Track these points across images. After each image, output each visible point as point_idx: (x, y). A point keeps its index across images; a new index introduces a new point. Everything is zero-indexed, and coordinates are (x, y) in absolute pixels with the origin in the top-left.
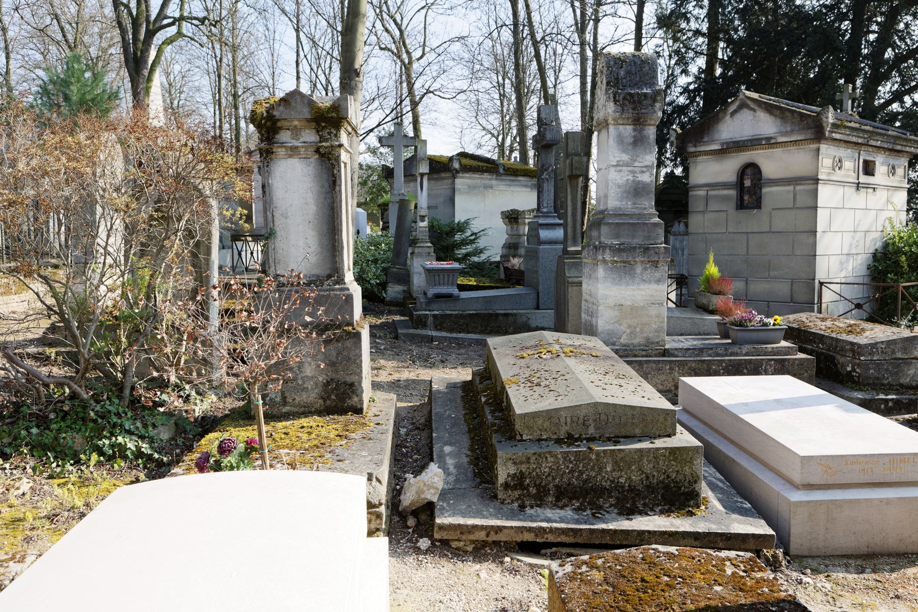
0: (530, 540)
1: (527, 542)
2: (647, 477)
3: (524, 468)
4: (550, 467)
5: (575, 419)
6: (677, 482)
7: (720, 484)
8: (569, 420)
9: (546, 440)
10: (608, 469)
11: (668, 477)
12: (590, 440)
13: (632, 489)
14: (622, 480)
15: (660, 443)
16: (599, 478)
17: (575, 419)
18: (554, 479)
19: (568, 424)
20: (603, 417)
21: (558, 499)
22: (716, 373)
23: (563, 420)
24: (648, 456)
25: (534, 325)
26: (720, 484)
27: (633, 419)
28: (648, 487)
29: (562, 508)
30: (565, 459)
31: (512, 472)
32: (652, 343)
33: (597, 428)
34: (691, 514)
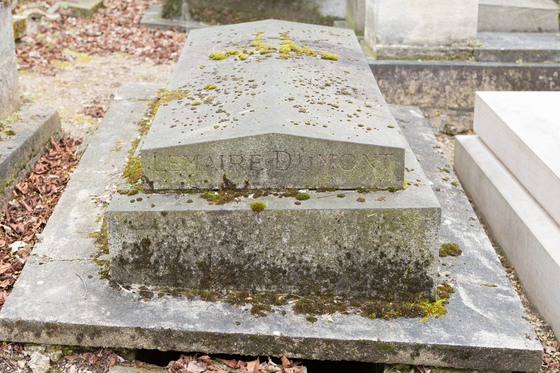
0: (146, 347)
1: (143, 350)
2: (348, 256)
3: (148, 234)
4: (190, 236)
5: (237, 159)
6: (396, 264)
7: (485, 262)
8: (227, 161)
9: (190, 191)
10: (285, 240)
11: (382, 255)
12: (258, 193)
13: (323, 273)
14: (307, 258)
15: (371, 202)
16: (270, 253)
17: (237, 159)
18: (197, 253)
19: (226, 167)
20: (283, 157)
21: (205, 284)
22: (544, 87)
23: (217, 161)
24: (349, 223)
25: (325, 12)
26: (485, 262)
27: (332, 161)
28: (350, 270)
29: (209, 298)
30: (214, 222)
31: (130, 241)
32: (456, 41)
33: (272, 175)
34: (416, 313)
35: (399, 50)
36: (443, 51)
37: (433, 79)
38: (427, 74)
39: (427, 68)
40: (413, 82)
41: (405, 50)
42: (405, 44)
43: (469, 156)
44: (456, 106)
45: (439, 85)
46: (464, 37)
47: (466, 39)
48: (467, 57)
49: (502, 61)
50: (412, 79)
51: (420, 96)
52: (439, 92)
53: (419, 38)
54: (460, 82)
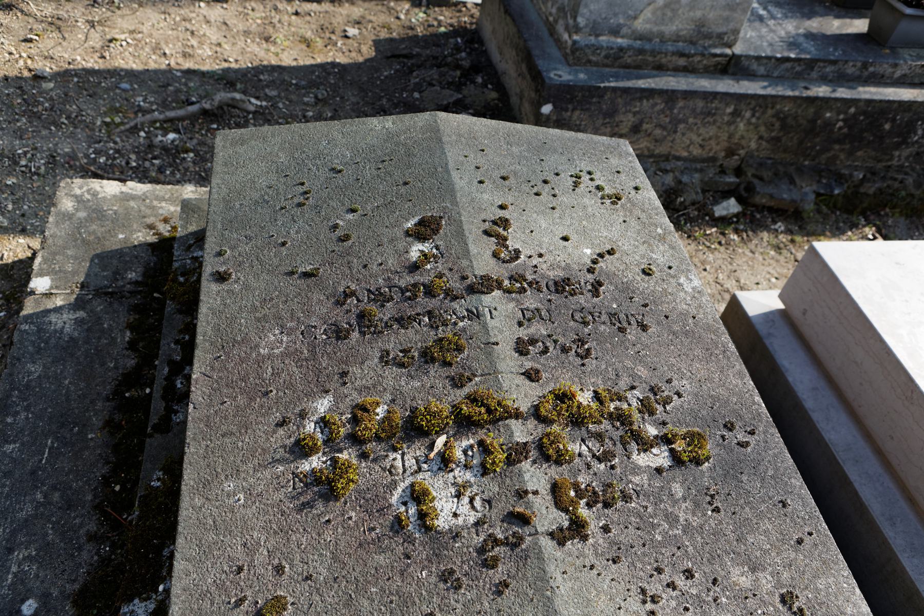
35: (612, 48)
36: (682, 55)
37: (662, 111)
38: (656, 104)
39: (659, 94)
40: (630, 116)
41: (621, 49)
42: (622, 37)
43: (818, 430)
44: (685, 154)
45: (670, 122)
46: (723, 29)
47: (726, 33)
48: (904, 212)
49: (793, 90)
50: (630, 111)
51: (635, 139)
52: (665, 133)
53: (648, 26)
54: (704, 119)
